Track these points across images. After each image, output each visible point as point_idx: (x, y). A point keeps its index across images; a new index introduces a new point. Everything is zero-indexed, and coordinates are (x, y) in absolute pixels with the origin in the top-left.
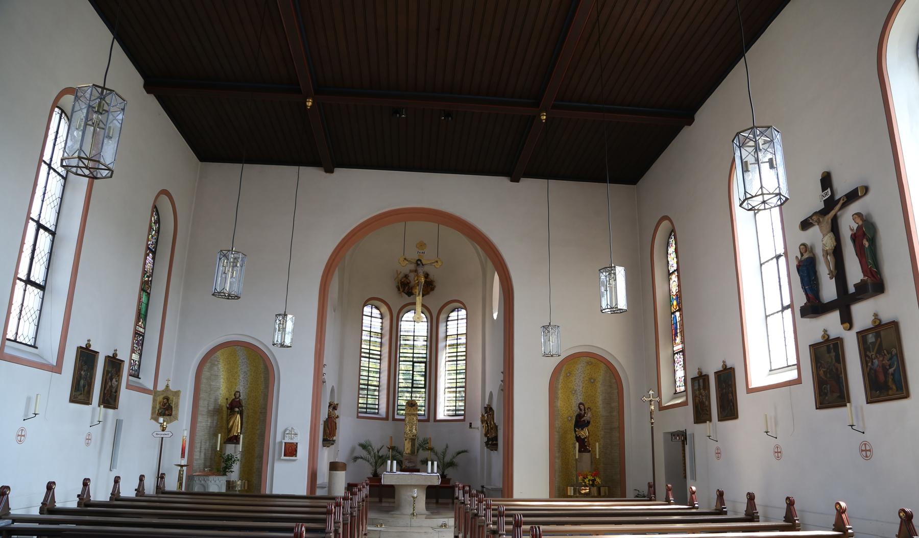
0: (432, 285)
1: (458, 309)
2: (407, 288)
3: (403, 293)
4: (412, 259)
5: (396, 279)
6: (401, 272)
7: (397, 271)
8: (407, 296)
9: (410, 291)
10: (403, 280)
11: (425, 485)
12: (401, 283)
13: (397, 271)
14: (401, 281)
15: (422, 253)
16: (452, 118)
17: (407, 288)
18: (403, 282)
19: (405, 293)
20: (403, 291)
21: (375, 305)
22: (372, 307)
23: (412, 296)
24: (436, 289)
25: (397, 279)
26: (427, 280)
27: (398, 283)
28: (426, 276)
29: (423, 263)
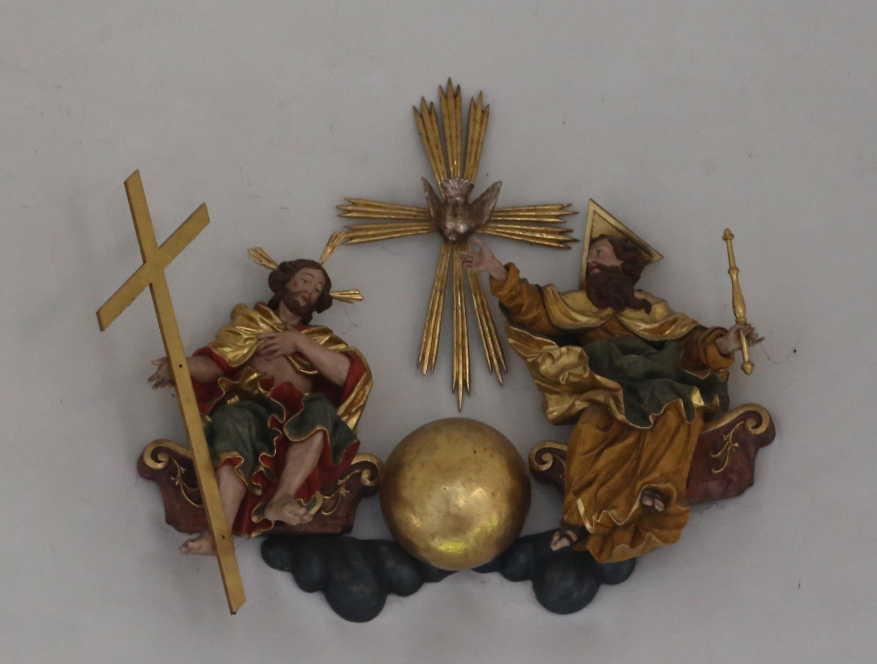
10: (232, 354)
14: (205, 353)
18: (232, 372)
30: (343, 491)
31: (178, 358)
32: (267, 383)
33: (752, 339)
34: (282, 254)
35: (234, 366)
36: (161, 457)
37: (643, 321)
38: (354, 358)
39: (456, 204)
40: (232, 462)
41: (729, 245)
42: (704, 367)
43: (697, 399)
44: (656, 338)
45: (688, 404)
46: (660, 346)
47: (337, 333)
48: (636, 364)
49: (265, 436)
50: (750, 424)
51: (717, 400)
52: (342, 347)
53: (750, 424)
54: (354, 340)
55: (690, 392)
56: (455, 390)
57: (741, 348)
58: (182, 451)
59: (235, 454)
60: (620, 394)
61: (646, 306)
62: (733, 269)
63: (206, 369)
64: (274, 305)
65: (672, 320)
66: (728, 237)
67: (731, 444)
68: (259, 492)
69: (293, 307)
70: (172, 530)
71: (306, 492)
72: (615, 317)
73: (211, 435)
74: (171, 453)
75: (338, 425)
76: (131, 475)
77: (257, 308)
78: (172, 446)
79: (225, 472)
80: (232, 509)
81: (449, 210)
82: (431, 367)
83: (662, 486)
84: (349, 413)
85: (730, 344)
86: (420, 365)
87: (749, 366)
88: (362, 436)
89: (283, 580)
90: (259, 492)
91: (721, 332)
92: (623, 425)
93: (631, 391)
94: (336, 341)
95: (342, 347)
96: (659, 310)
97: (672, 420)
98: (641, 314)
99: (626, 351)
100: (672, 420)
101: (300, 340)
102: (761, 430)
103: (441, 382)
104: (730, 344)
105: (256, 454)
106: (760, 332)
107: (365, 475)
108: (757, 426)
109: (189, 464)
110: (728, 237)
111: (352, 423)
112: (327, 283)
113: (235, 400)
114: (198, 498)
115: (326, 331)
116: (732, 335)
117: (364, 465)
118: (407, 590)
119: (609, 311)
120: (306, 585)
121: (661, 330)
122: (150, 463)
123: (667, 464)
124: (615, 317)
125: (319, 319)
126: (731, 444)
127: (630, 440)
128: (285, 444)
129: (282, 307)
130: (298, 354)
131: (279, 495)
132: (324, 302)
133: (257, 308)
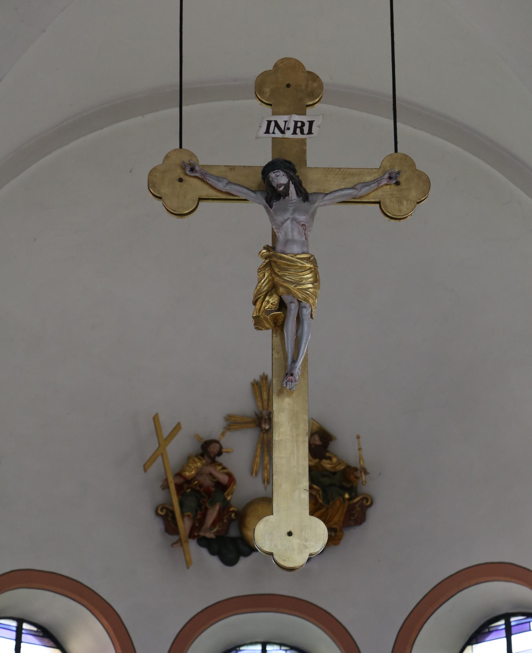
0: (353, 491)
1: (507, 617)
2: (212, 515)
3: (193, 545)
4: (232, 168)
5: (152, 459)
6: (178, 428)
7: (156, 418)
8: (214, 561)
9: (233, 532)
10: (189, 474)
11: (262, 166)
12: (179, 488)
13: (156, 418)
14: (179, 475)
15: (299, 127)
16: (350, 499)
17: (212, 515)
18: (189, 481)
19: (203, 542)
20: (191, 536)
21: (42, 619)
22: (19, 632)
23: (244, 563)
24: (373, 514)
25: (156, 467)
26: (327, 464)
27: (165, 486)
28: (317, 441)
29: (310, 189)
30: (225, 521)
31: (171, 479)
32: (201, 486)
33: (366, 473)
34: (207, 438)
35: (189, 479)
36: (164, 511)
37: (328, 464)
38: (230, 475)
39: (265, 419)
40: (189, 516)
41: (371, 183)
42: (349, 481)
43: (347, 496)
44: (333, 470)
45: (344, 498)
46: (334, 473)
47: (225, 464)
48: (326, 481)
49: (199, 506)
50: (365, 501)
51: (353, 494)
52: (226, 471)
53: (365, 501)
54: (231, 469)
55: (344, 494)
56: (264, 482)
57: (362, 476)
58: (170, 508)
59: (189, 513)
60: (321, 492)
61: (330, 458)
62: (360, 449)
63: (180, 480)
64: (202, 455)
65: (339, 462)
66: (358, 437)
67: (358, 509)
68: (197, 525)
69: (210, 457)
70: (167, 534)
71: (214, 524)
72: (319, 462)
73: (181, 505)
74: (167, 509)
75: (225, 499)
76: (153, 515)
77: (197, 456)
78: (168, 506)
79: (186, 519)
80: (188, 531)
81: (263, 421)
82: (256, 474)
83: (334, 526)
84: (228, 495)
85: (358, 474)
86: (252, 474)
87: (364, 483)
88: (232, 502)
89: (204, 552)
90: (197, 525)
91: (356, 469)
92: (321, 504)
93: (324, 491)
94: (224, 468)
95: (226, 471)
96: (335, 460)
97: (338, 503)
98: (328, 461)
99: (323, 476)
100: (338, 503)
101: (211, 469)
102: (369, 503)
103: (259, 478)
104: (358, 474)
105: (196, 512)
106: (368, 470)
107: (233, 515)
108: (367, 502)
109: (173, 512)
110: (358, 437)
111: (229, 498)
112: (221, 448)
113: (189, 490)
114: (176, 525)
115: (220, 464)
116: (359, 472)
117: (233, 511)
118: (247, 555)
119: (317, 460)
120: (212, 553)
121: (335, 467)
122: (160, 512)
123: (336, 519)
124: (319, 462)
125: (219, 459)
126: (358, 509)
127: (324, 510)
128: (206, 509)
129: (205, 456)
130: (211, 474)
131: (204, 528)
132: (220, 453)
133: (197, 456)
